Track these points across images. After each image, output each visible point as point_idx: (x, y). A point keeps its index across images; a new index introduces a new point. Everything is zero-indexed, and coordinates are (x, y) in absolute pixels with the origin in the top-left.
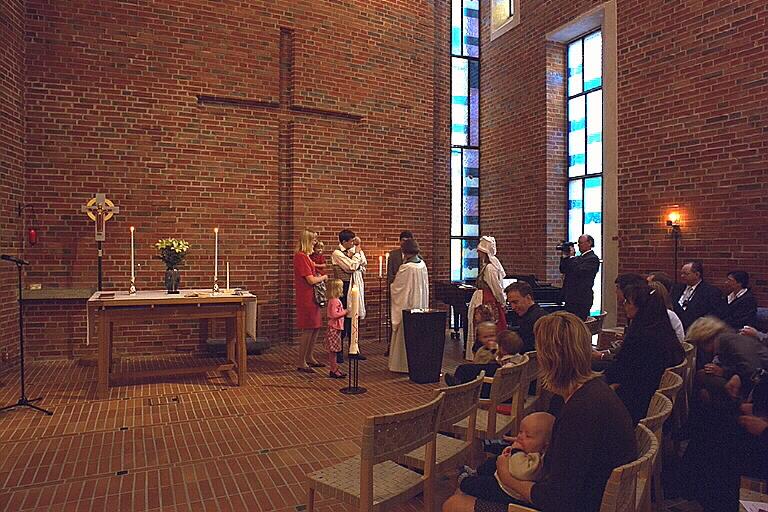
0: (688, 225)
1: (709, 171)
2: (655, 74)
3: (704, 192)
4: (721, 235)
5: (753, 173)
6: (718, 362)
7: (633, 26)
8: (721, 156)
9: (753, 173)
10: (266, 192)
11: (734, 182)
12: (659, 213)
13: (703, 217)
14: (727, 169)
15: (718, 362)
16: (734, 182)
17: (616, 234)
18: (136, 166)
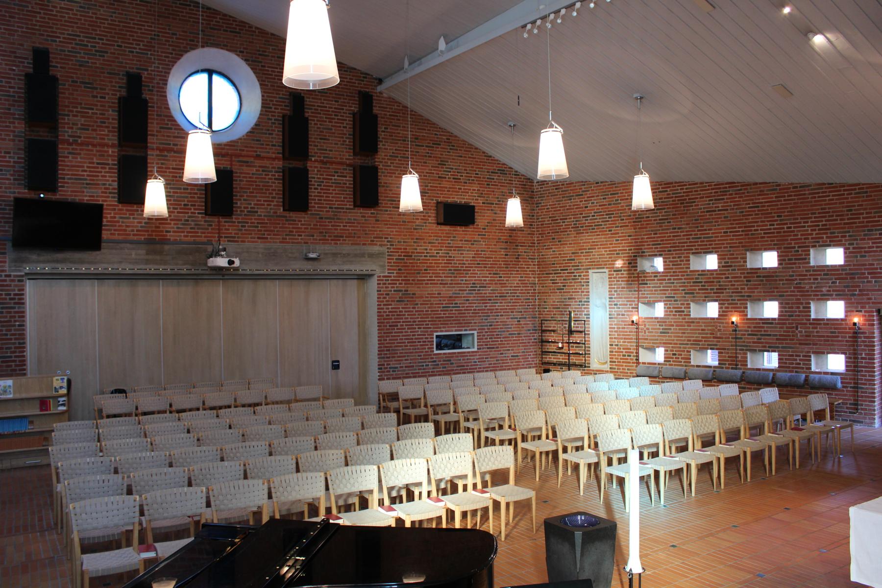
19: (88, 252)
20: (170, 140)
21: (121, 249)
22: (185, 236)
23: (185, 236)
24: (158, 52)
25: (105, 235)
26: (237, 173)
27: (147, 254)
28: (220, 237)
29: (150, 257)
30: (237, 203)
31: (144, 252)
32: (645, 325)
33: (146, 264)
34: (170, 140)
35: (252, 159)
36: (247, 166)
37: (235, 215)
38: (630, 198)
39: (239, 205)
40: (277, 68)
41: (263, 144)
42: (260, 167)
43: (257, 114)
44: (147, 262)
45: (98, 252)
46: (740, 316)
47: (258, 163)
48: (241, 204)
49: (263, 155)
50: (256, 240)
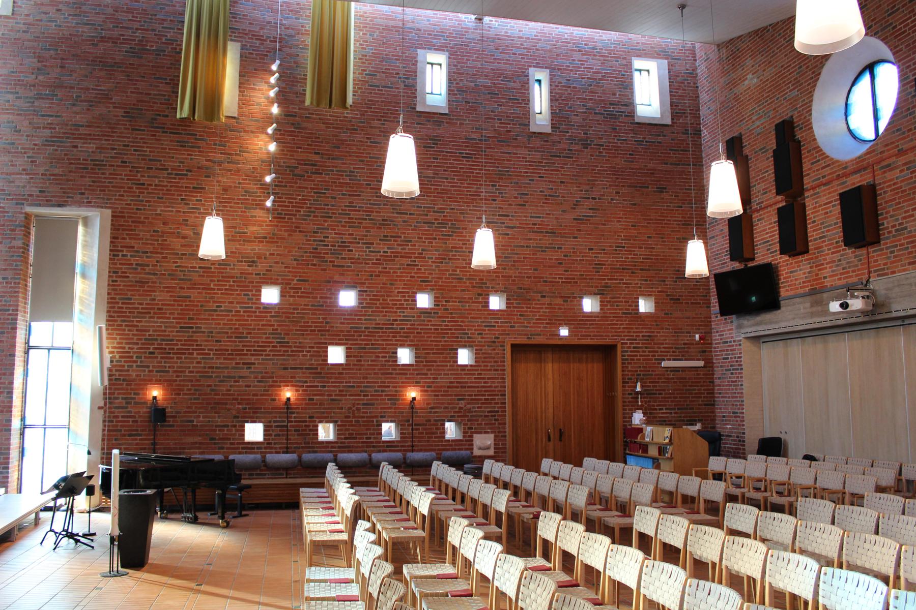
0: (164, 399)
1: (181, 363)
2: (141, 283)
3: (177, 376)
4: (188, 408)
5: (209, 368)
6: (302, 38)
7: (124, 239)
8: (190, 354)
9: (209, 368)
10: (424, 211)
11: (197, 372)
12: (143, 389)
13: (175, 394)
14: (193, 363)
15: (302, 38)
16: (197, 372)
17: (102, 404)
18: (294, 220)
19: (747, 317)
20: (380, 248)
21: (794, 304)
22: (840, 279)
23: (840, 279)
24: (485, 151)
25: (783, 293)
26: (880, 184)
27: (812, 306)
28: (869, 272)
29: (814, 309)
30: (883, 224)
31: (808, 305)
32: (358, 409)
33: (811, 317)
34: (380, 248)
35: (894, 159)
36: (890, 170)
37: (884, 239)
38: (380, 181)
39: (886, 225)
40: (510, 124)
41: (356, 239)
42: (904, 164)
43: (815, 114)
44: (812, 315)
45: (779, 311)
46: (422, 391)
47: (901, 160)
48: (888, 223)
49: (905, 147)
50: (203, 343)
